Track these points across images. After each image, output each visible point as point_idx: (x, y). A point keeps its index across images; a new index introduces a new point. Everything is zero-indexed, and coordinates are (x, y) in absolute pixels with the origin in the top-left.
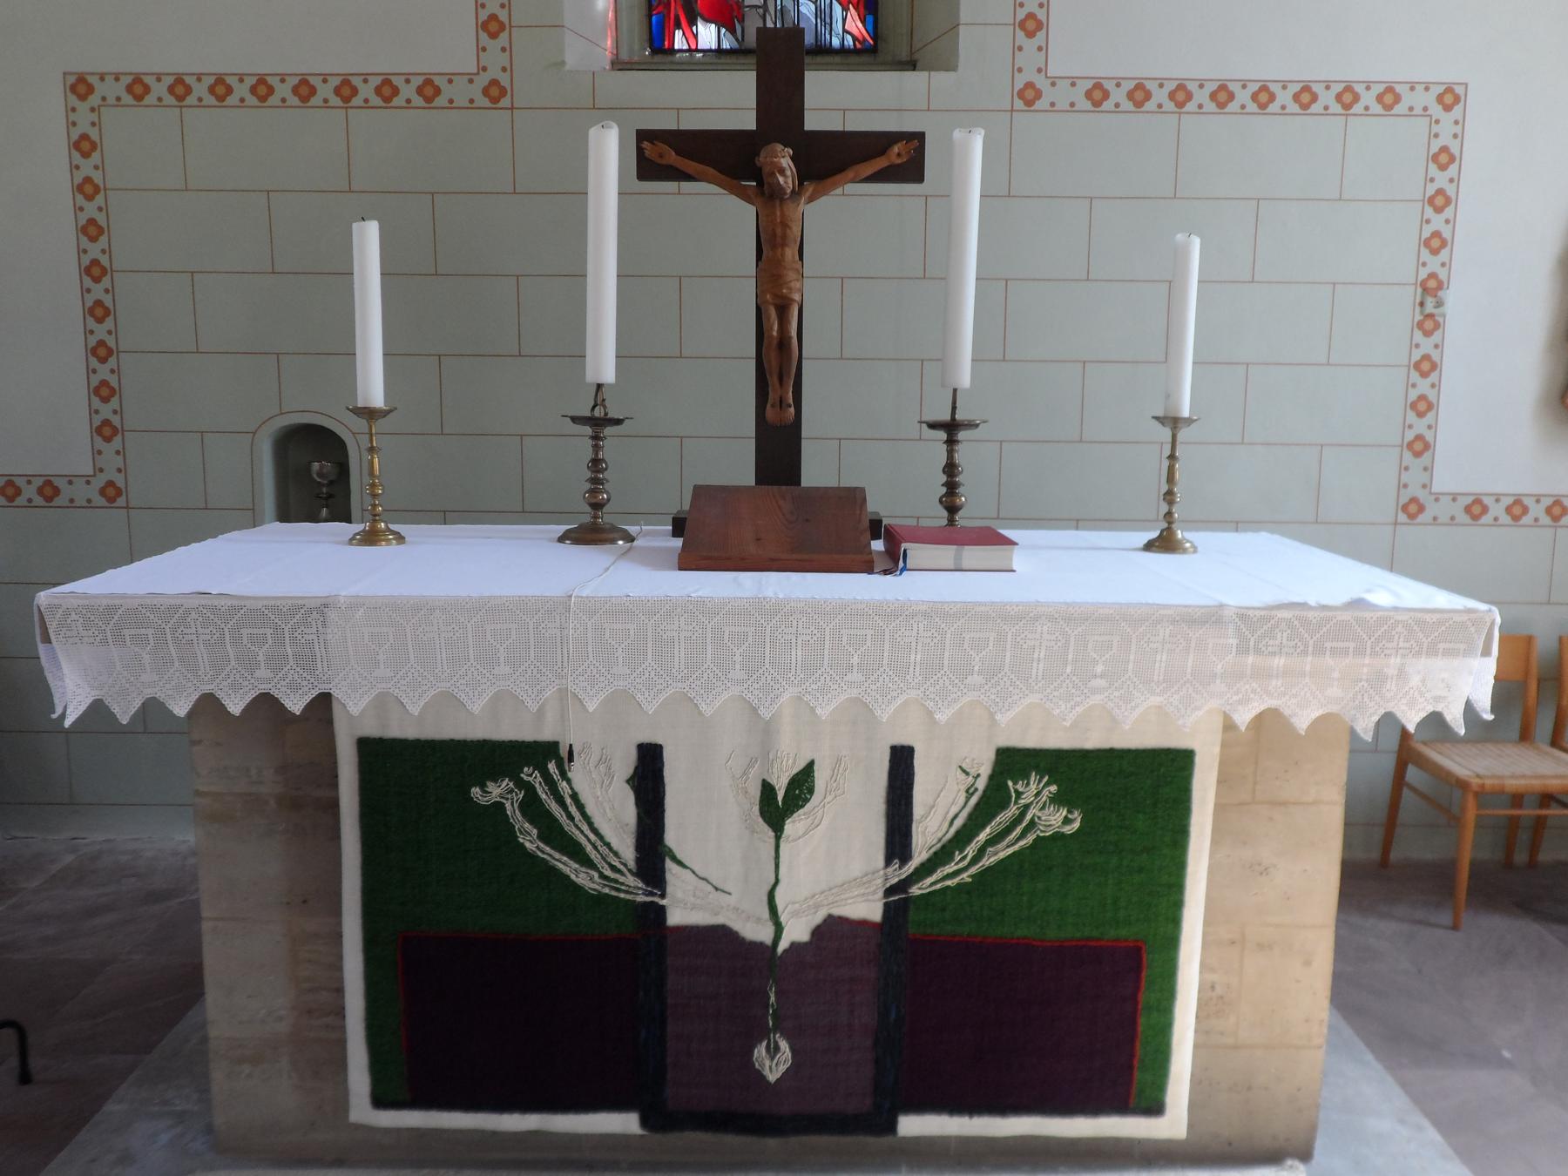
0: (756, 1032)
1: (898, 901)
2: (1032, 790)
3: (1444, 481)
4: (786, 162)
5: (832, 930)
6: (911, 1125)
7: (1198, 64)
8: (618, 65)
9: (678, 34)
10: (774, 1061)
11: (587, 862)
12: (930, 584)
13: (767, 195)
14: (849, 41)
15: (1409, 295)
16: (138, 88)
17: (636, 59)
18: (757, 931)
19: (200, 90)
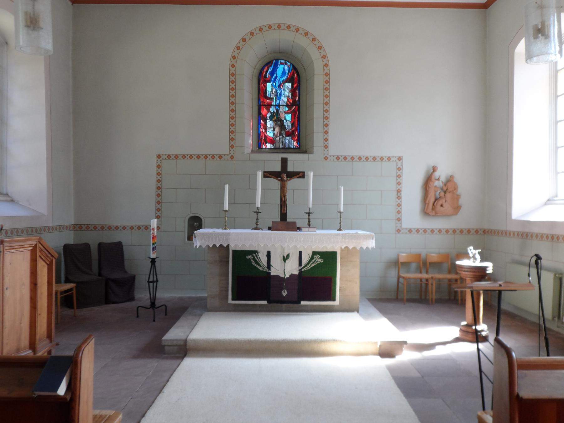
0: (282, 289)
1: (300, 272)
2: (317, 257)
3: (404, 226)
4: (285, 176)
5: (292, 276)
6: (303, 303)
7: (356, 153)
8: (253, 151)
10: (285, 293)
11: (261, 266)
12: (305, 232)
13: (282, 180)
15: (395, 193)
16: (169, 156)
18: (282, 276)
19: (180, 157)
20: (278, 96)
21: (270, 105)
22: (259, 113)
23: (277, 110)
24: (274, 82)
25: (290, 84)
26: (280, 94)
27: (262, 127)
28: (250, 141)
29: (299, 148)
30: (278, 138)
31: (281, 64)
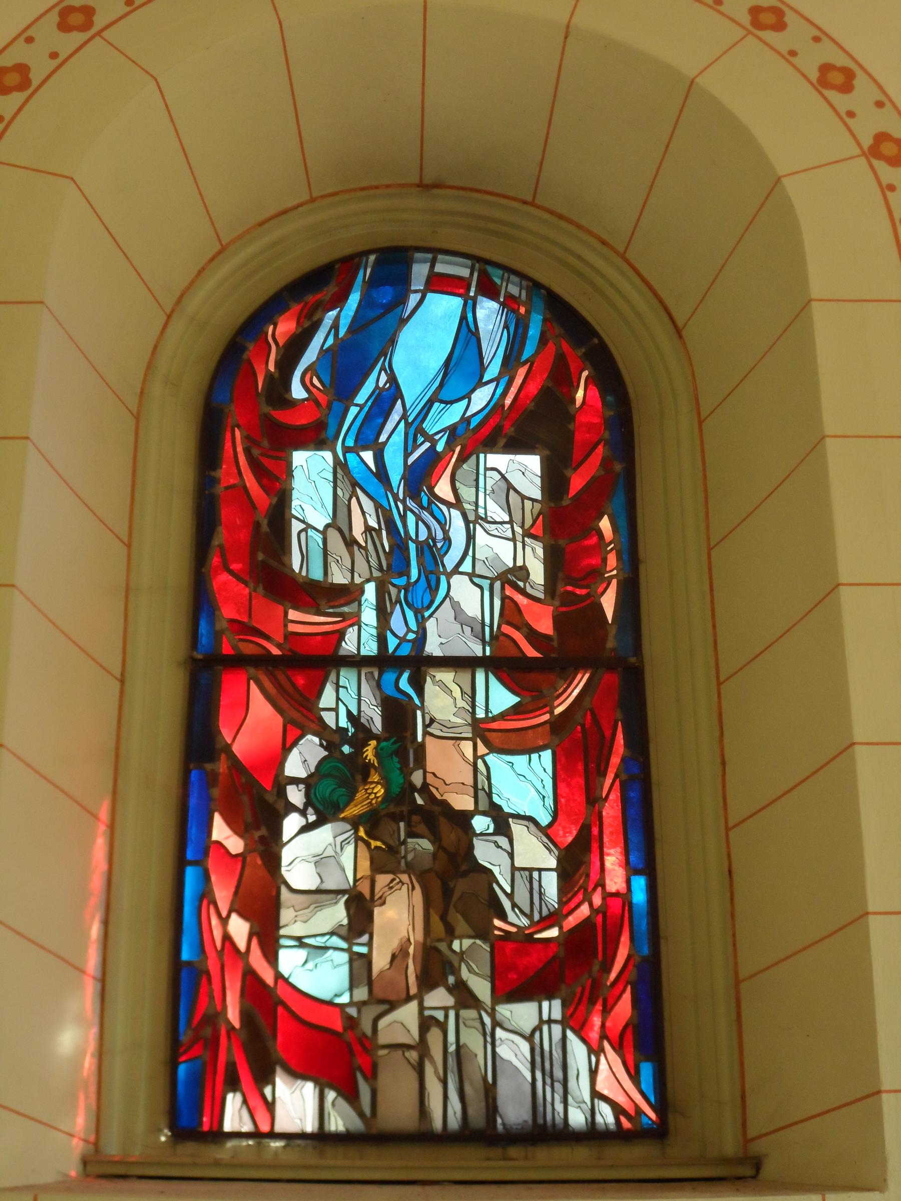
8: (100, 1168)
9: (233, 1102)
14: (606, 1116)
17: (137, 1152)
20: (410, 567)
21: (319, 660)
22: (200, 741)
23: (399, 715)
24: (369, 437)
25: (533, 462)
26: (432, 553)
27: (223, 895)
28: (72, 1039)
29: (659, 1133)
30: (408, 1014)
31: (439, 284)
